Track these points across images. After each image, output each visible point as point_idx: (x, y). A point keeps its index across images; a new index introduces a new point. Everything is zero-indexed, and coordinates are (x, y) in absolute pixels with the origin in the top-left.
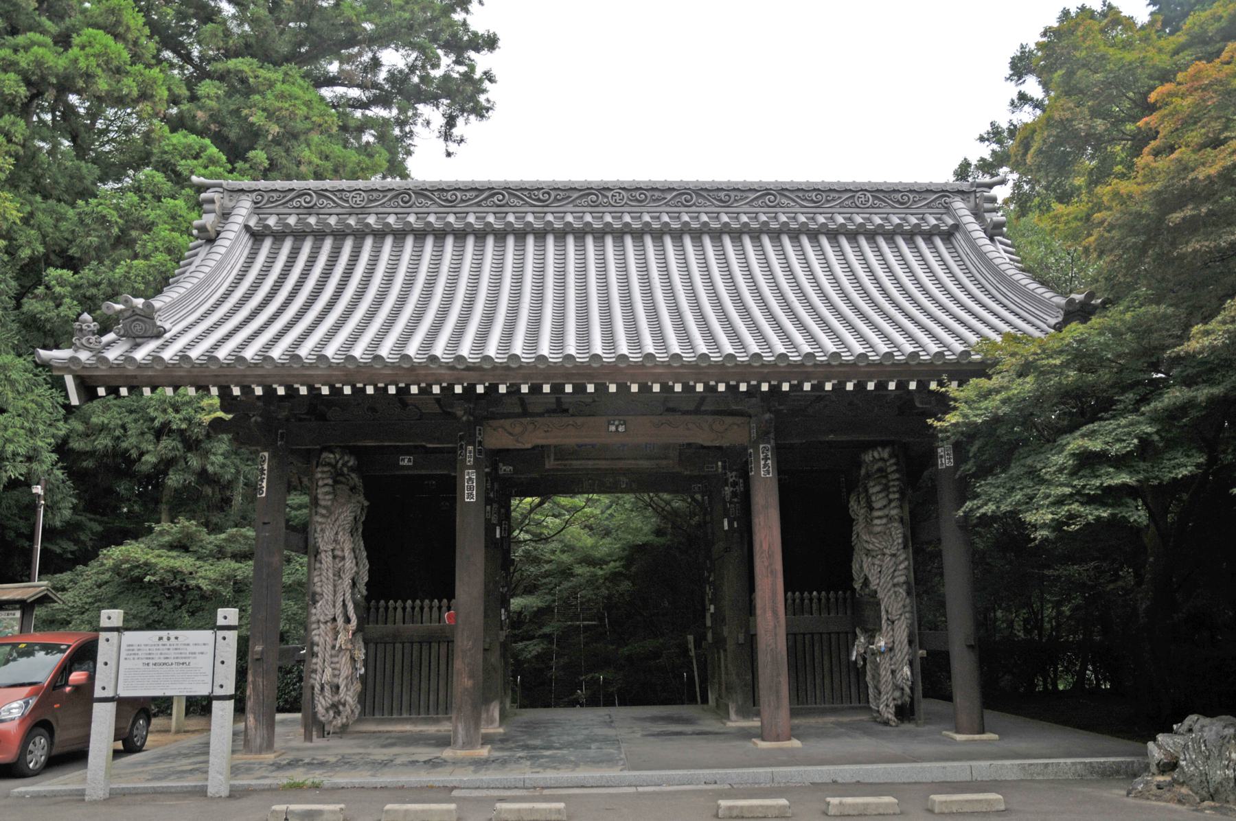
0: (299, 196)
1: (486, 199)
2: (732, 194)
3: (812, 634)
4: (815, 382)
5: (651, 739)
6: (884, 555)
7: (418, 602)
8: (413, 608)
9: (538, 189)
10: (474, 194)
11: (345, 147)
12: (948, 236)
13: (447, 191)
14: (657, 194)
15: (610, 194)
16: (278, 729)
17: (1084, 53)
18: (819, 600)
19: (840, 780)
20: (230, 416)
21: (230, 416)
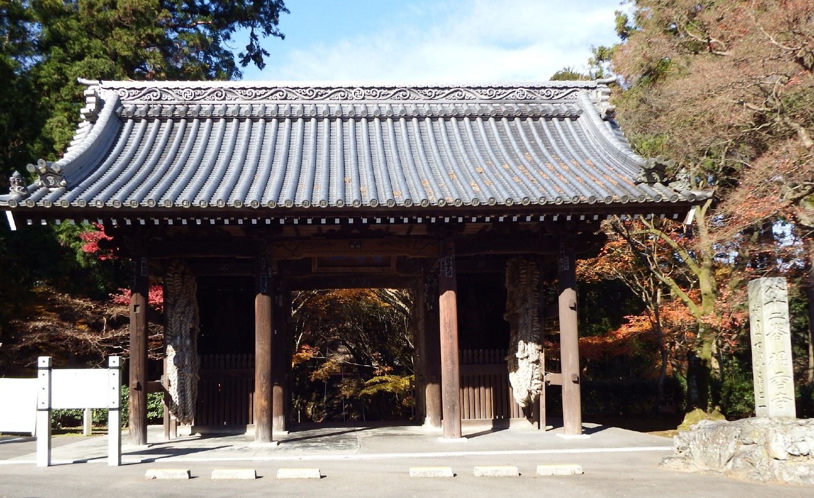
0: (149, 92)
1: (272, 95)
2: (434, 91)
3: (490, 363)
4: (506, 216)
5: (377, 438)
6: (767, 97)
7: (234, 355)
8: (231, 359)
9: (306, 88)
10: (264, 91)
11: (799, 192)
12: (574, 118)
13: (247, 89)
14: (384, 91)
15: (353, 91)
16: (149, 433)
17: (711, 451)
18: (484, 355)
19: (486, 474)
20: (111, 238)
21: (111, 238)
